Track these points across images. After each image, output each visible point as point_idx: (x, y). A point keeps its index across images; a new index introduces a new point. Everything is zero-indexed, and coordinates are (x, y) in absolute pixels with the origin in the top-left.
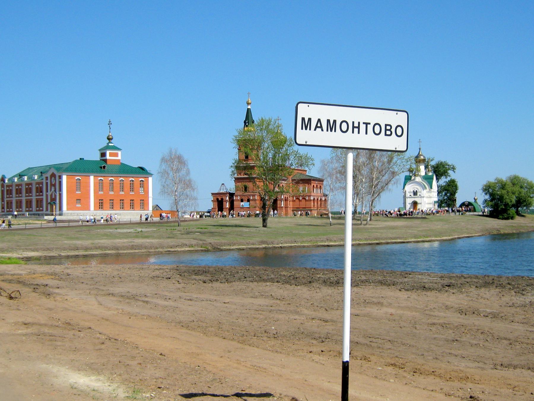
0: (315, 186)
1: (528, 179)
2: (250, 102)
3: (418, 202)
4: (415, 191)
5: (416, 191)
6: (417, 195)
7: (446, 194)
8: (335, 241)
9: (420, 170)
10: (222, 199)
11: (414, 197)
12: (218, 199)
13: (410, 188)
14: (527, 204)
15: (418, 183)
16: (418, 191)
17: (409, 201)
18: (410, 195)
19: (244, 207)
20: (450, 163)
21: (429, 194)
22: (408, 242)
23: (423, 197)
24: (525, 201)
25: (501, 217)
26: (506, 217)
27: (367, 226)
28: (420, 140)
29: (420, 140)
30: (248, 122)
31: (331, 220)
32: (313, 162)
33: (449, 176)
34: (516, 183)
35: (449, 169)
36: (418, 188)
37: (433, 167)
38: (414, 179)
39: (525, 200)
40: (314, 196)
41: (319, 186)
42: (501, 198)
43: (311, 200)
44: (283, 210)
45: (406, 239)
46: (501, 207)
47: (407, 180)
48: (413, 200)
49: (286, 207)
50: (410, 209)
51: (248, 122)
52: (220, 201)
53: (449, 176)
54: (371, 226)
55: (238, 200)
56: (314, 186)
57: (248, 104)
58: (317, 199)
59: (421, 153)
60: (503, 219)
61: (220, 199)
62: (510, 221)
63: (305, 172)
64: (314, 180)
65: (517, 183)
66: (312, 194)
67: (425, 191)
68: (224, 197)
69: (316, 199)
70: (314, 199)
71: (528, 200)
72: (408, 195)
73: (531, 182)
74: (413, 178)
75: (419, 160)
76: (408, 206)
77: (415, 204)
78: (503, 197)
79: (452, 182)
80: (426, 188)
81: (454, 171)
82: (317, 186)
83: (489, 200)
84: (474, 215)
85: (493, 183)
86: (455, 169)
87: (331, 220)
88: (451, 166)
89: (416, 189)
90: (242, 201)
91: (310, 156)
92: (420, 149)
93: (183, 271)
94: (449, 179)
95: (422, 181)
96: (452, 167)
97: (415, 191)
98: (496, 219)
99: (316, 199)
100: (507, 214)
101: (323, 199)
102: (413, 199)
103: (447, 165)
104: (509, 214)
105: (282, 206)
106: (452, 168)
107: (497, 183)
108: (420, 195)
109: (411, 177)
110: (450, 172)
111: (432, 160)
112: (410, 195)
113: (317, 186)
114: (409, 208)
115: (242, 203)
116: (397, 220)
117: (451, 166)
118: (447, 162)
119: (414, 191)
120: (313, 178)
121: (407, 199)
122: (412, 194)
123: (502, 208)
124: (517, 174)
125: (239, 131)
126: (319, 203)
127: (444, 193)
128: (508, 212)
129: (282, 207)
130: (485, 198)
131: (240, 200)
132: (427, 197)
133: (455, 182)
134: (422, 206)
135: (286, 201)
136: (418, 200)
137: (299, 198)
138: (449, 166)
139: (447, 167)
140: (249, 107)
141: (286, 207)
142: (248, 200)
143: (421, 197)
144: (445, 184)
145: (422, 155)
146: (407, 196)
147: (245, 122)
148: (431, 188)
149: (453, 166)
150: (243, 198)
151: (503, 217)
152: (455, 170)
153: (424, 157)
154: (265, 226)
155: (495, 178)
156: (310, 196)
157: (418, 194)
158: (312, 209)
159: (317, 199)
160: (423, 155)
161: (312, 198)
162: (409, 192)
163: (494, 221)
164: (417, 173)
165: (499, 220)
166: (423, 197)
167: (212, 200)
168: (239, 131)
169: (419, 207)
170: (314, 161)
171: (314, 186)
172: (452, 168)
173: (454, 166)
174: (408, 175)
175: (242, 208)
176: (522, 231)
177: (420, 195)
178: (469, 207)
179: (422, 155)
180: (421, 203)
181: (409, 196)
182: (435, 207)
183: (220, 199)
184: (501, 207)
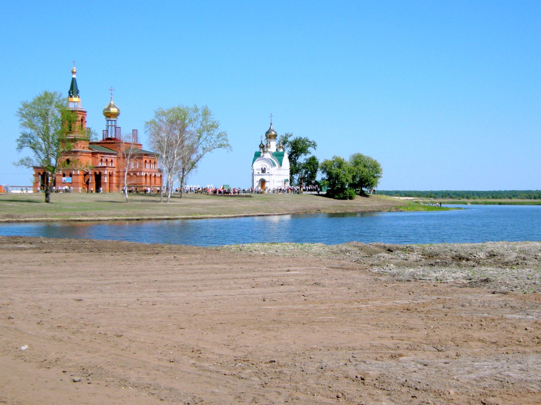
0: (148, 161)
1: (373, 158)
2: (75, 71)
3: (267, 180)
4: (263, 168)
5: (265, 168)
6: (265, 173)
7: (306, 173)
8: (91, 216)
9: (270, 146)
10: (100, 173)
11: (262, 175)
12: (95, 173)
13: (258, 165)
14: (369, 184)
15: (267, 160)
16: (266, 168)
17: (257, 179)
18: (258, 173)
19: (66, 182)
20: (310, 140)
21: (279, 172)
23: (272, 175)
24: (367, 181)
25: (336, 196)
26: (342, 196)
27: (168, 203)
28: (271, 114)
29: (271, 114)
30: (72, 93)
31: (127, 196)
32: (97, 137)
33: (310, 153)
34: (359, 161)
35: (309, 146)
36: (268, 166)
37: (291, 143)
38: (263, 156)
39: (367, 179)
40: (146, 172)
41: (153, 161)
42: (337, 176)
43: (142, 176)
44: (106, 186)
45: (175, 216)
46: (337, 186)
47: (257, 157)
48: (260, 177)
49: (110, 183)
50: (258, 187)
51: (72, 93)
52: (98, 175)
53: (310, 153)
54: (171, 203)
55: (60, 175)
56: (146, 161)
57: (73, 73)
58: (151, 175)
59: (272, 128)
60: (339, 199)
61: (98, 173)
62: (348, 201)
63: (140, 146)
64: (146, 155)
65: (360, 162)
66: (144, 170)
67: (274, 168)
68: (102, 172)
69: (148, 174)
70: (146, 175)
72: (256, 172)
73: (376, 161)
74: (262, 154)
75: (270, 135)
76: (256, 184)
78: (338, 176)
79: (313, 160)
80: (276, 166)
81: (314, 148)
83: (327, 178)
84: (311, 194)
85: (330, 162)
86: (316, 146)
87: (127, 196)
88: (312, 142)
89: (265, 167)
90: (64, 175)
91: (94, 131)
92: (271, 124)
94: (308, 156)
95: (272, 157)
97: (263, 168)
98: (332, 199)
99: (148, 174)
100: (344, 194)
101: (158, 175)
102: (261, 176)
103: (307, 141)
104: (346, 194)
105: (106, 181)
106: (313, 145)
107: (334, 161)
108: (268, 173)
110: (310, 149)
111: (290, 136)
112: (258, 173)
113: (150, 161)
114: (256, 186)
115: (64, 178)
116: (213, 196)
117: (312, 142)
118: (308, 139)
119: (262, 168)
120: (144, 153)
121: (255, 176)
122: (260, 172)
123: (338, 188)
124: (361, 153)
125: (23, 103)
126: (153, 179)
127: (304, 171)
128: (344, 192)
129: (106, 183)
130: (322, 177)
131: (62, 175)
132: (276, 175)
133: (317, 159)
134: (270, 185)
136: (266, 178)
137: (130, 173)
138: (309, 142)
139: (308, 143)
140: (74, 76)
141: (110, 183)
142: (71, 175)
143: (269, 175)
144: (305, 161)
145: (273, 131)
147: (69, 93)
148: (281, 165)
149: (314, 143)
150: (66, 173)
151: (339, 197)
152: (316, 147)
153: (275, 132)
154: (47, 201)
155: (333, 156)
156: (141, 172)
157: (267, 171)
158: (143, 185)
159: (151, 175)
160: (275, 130)
161: (143, 174)
162: (258, 170)
163: (325, 200)
164: (266, 150)
165: (335, 200)
166: (272, 175)
167: (34, 175)
169: (267, 185)
171: (146, 161)
172: (313, 145)
173: (315, 142)
174: (259, 151)
175: (64, 184)
176: (348, 211)
177: (268, 173)
179: (273, 131)
180: (269, 182)
181: (257, 173)
182: (286, 185)
183: (98, 173)
184: (337, 186)
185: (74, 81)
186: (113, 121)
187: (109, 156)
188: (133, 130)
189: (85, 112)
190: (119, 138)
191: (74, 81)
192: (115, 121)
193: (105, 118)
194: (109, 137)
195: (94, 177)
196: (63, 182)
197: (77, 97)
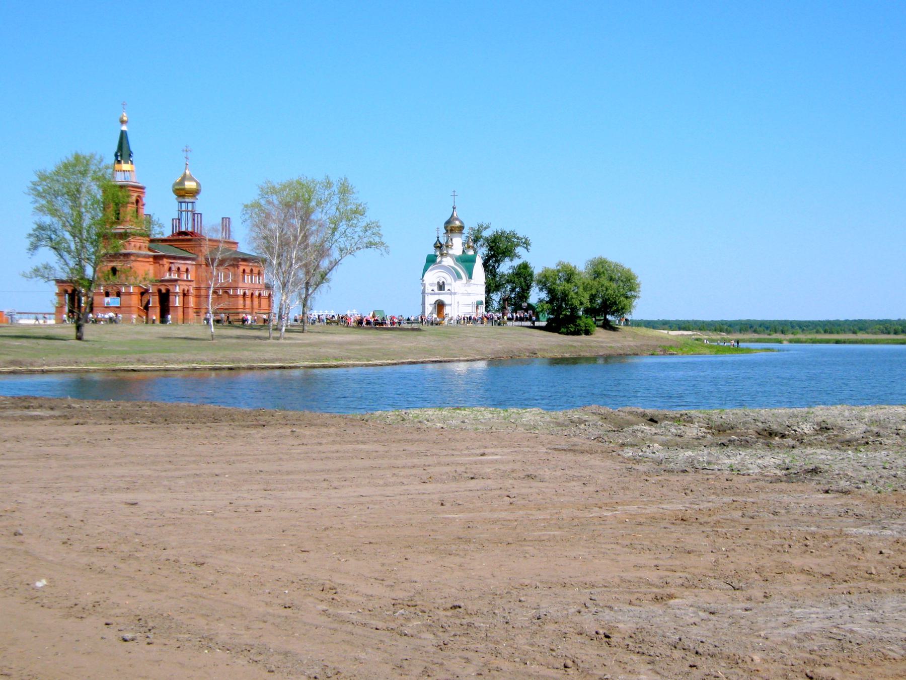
1: (624, 266)
2: (125, 119)
3: (446, 302)
4: (441, 282)
5: (443, 282)
6: (444, 290)
7: (513, 290)
8: (152, 363)
9: (452, 246)
10: (168, 291)
11: (439, 294)
12: (160, 291)
13: (433, 276)
14: (618, 308)
15: (447, 269)
16: (445, 282)
17: (431, 300)
18: (433, 290)
19: (111, 306)
20: (520, 235)
21: (467, 288)
22: (291, 368)
23: (455, 293)
24: (615, 303)
25: (563, 330)
26: (572, 330)
27: (282, 341)
28: (454, 191)
29: (454, 191)
30: (121, 156)
31: (213, 330)
32: (162, 230)
33: (519, 257)
34: (601, 271)
35: (518, 245)
36: (448, 279)
37: (487, 240)
38: (440, 262)
39: (615, 301)
40: (244, 288)
41: (256, 271)
42: (565, 295)
43: (237, 296)
44: (177, 312)
45: (292, 363)
46: (564, 313)
47: (430, 263)
48: (436, 298)
49: (185, 307)
51: (121, 156)
52: (164, 293)
53: (519, 257)
54: (287, 341)
56: (244, 270)
57: (123, 122)
58: (252, 294)
59: (455, 215)
60: (567, 334)
61: (164, 291)
62: (583, 337)
63: (234, 246)
64: (244, 260)
65: (603, 272)
66: (241, 285)
67: (459, 283)
68: (171, 288)
69: (248, 293)
70: (245, 294)
71: (620, 302)
72: (428, 289)
73: (629, 270)
74: (439, 259)
75: (452, 227)
76: (429, 309)
77: (440, 306)
78: (567, 296)
79: (524, 268)
80: (462, 278)
81: (527, 248)
82: (252, 270)
83: (548, 299)
84: (521, 326)
85: (553, 271)
86: (529, 245)
87: (213, 330)
88: (522, 239)
89: (443, 280)
90: (107, 294)
92: (454, 208)
93: (498, 523)
94: (517, 262)
95: (455, 264)
96: (524, 240)
97: (441, 282)
98: (556, 334)
99: (248, 293)
100: (576, 326)
101: (265, 293)
102: (437, 296)
103: (514, 237)
104: (579, 325)
105: (177, 304)
106: (524, 243)
107: (559, 271)
108: (449, 290)
109: (437, 256)
110: (519, 250)
111: (486, 228)
112: (433, 290)
113: (252, 270)
114: (429, 312)
115: (107, 300)
116: (357, 330)
117: (522, 239)
118: (515, 233)
119: (438, 282)
120: (241, 257)
121: (426, 296)
122: (436, 288)
123: (565, 315)
124: (604, 256)
125: (39, 173)
126: (256, 301)
127: (509, 287)
128: (576, 322)
129: (177, 307)
130: (539, 297)
131: (104, 293)
132: (463, 294)
133: (530, 268)
134: (453, 310)
135: (186, 297)
136: (445, 298)
137: (218, 291)
138: (518, 238)
139: (515, 240)
140: (124, 128)
141: (185, 307)
142: (119, 294)
143: (451, 294)
144: (511, 271)
145: (457, 219)
146: (426, 292)
147: (116, 156)
148: (470, 277)
149: (526, 240)
150: (110, 290)
151: (567, 331)
152: (529, 247)
153: (461, 222)
154: (79, 338)
155: (557, 261)
156: (236, 288)
157: (446, 288)
158: (240, 311)
159: (252, 294)
160: (460, 218)
161: (240, 292)
162: (431, 285)
163: (545, 336)
164: (445, 252)
165: (561, 335)
166: (455, 293)
167: (57, 293)
168: (39, 173)
169: (447, 310)
170: (163, 229)
172: (524, 243)
173: (528, 239)
174: (434, 253)
175: (108, 308)
176: (582, 354)
177: (449, 290)
178: (529, 311)
179: (457, 219)
180: (450, 305)
181: (430, 291)
182: (479, 311)
183: (164, 291)
184: (564, 313)
185: (123, 136)
186: (189, 204)
187: (183, 262)
188: (223, 218)
189: (143, 188)
190: (199, 232)
191: (123, 136)
192: (192, 203)
193: (177, 199)
194: (183, 229)
195: (157, 298)
196: (106, 305)
197: (128, 163)
